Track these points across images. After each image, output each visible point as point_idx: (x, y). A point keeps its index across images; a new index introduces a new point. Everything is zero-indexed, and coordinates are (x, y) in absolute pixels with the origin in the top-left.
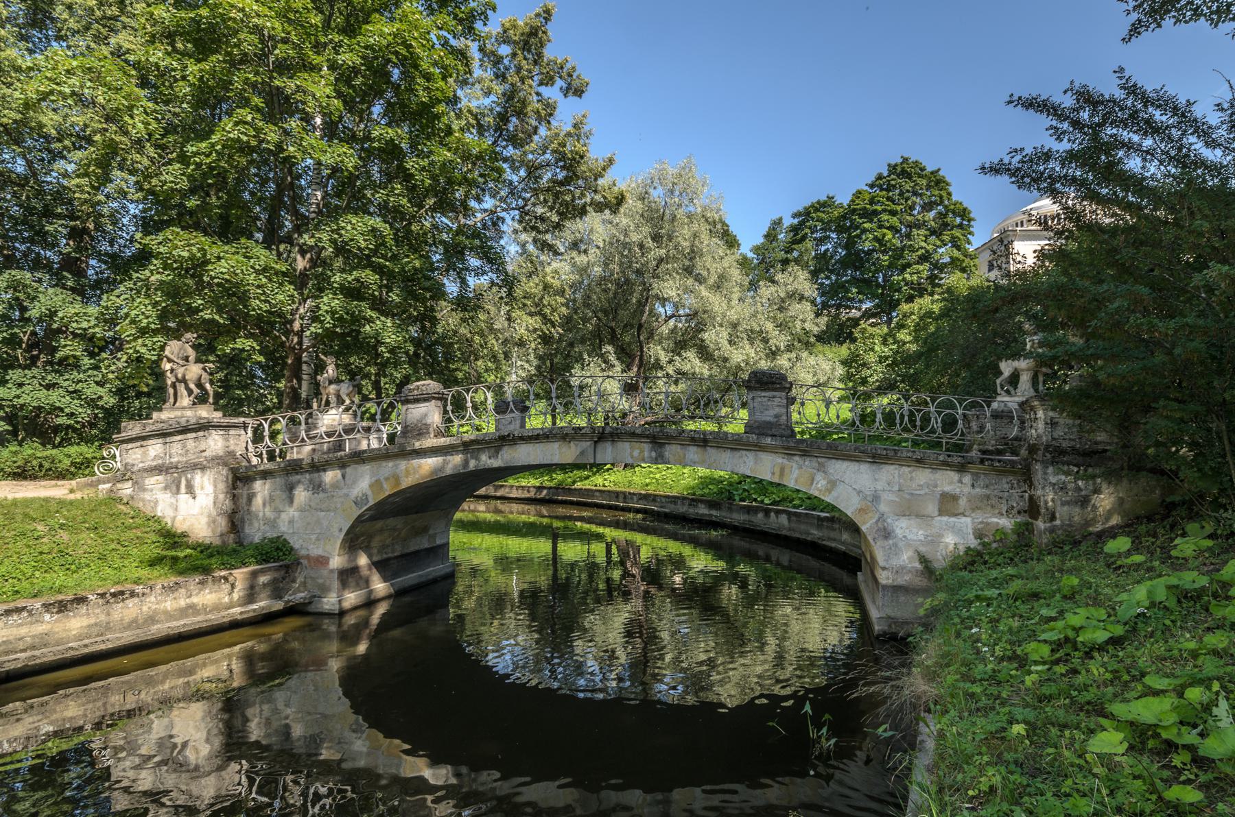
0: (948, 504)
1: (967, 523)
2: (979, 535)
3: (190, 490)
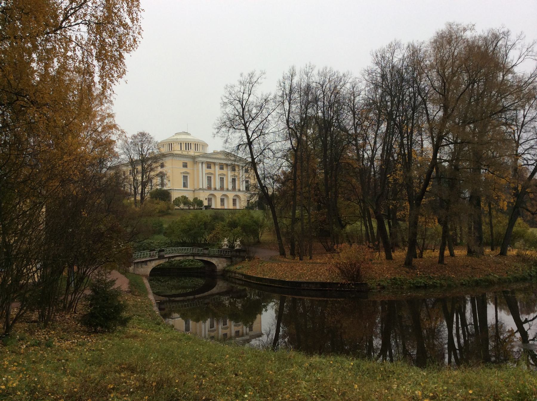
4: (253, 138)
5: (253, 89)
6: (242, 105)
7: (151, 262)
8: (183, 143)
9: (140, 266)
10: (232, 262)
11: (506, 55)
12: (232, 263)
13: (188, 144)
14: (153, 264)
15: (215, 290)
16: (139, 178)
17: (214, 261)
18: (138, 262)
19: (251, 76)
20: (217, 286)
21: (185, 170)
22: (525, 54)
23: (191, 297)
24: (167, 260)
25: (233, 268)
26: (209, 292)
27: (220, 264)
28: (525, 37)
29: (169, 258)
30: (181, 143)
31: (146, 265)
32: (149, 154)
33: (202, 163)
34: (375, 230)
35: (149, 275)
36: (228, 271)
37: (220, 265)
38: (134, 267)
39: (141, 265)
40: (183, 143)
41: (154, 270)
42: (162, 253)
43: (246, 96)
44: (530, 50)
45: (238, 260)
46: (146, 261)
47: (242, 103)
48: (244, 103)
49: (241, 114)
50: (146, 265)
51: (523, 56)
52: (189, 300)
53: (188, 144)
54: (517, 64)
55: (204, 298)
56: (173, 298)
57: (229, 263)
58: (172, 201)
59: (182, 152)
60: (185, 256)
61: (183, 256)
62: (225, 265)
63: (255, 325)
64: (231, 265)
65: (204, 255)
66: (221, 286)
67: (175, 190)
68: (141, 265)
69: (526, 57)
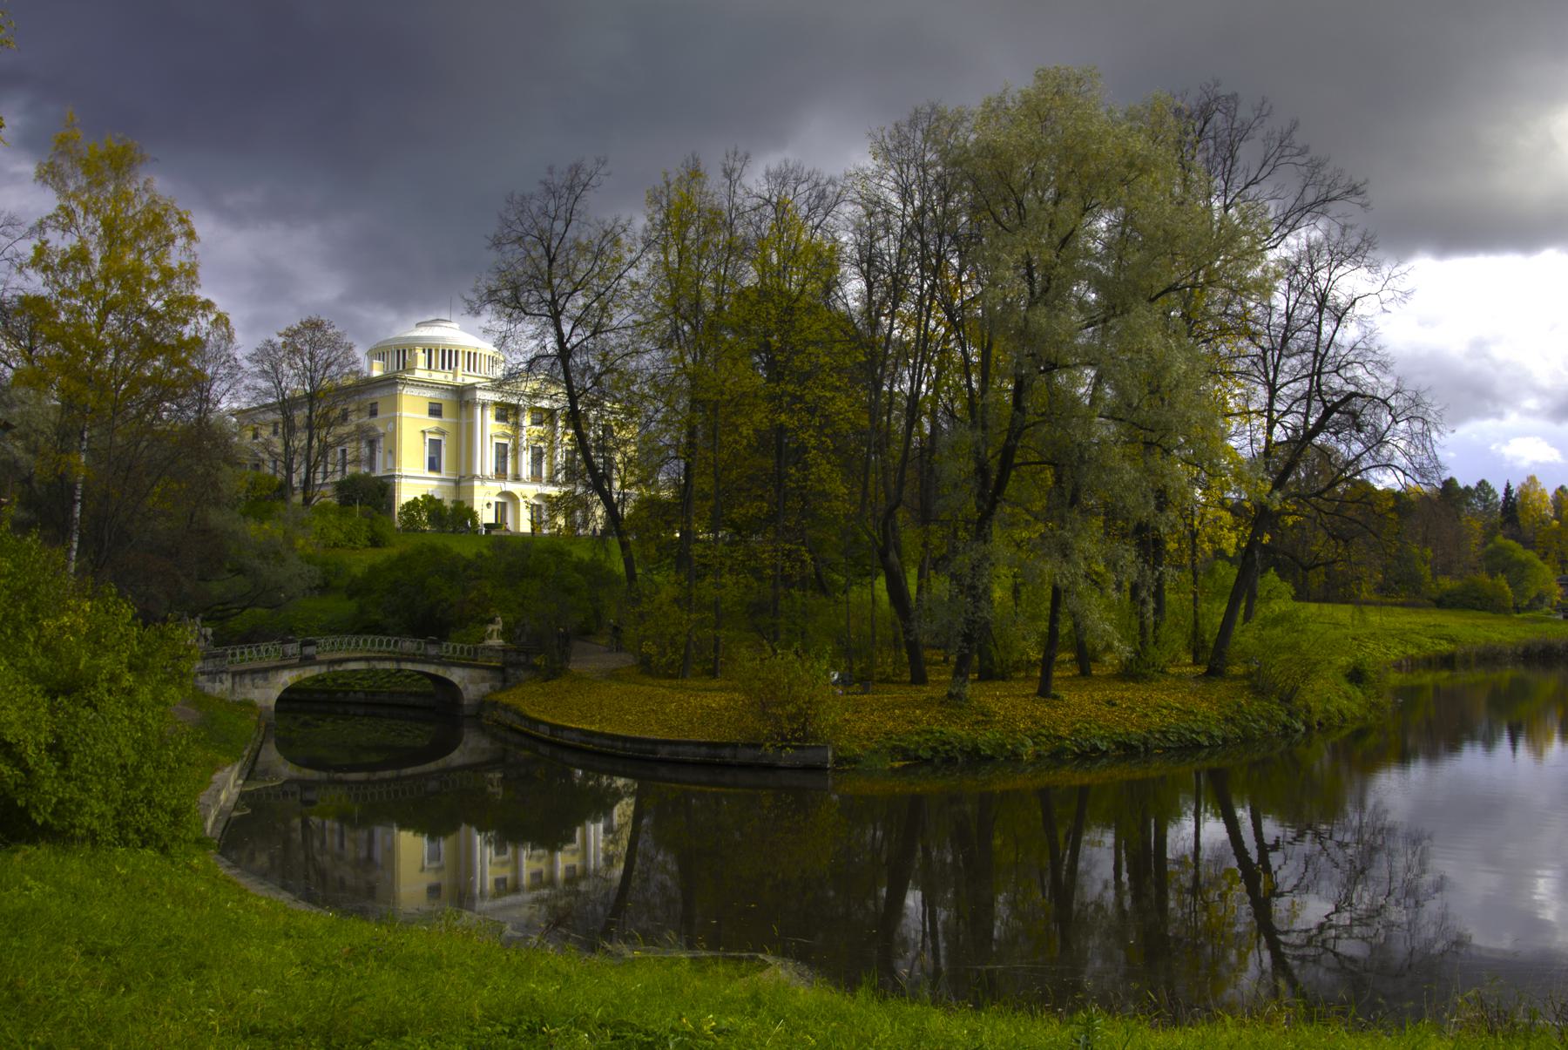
0: (483, 680)
1: (488, 685)
2: (491, 687)
3: (221, 681)
4: (574, 340)
5: (578, 207)
6: (548, 251)
7: (270, 675)
8: (437, 350)
9: (247, 680)
10: (505, 681)
11: (1232, 156)
12: (506, 684)
13: (450, 352)
14: (287, 678)
15: (456, 758)
16: (300, 440)
17: (456, 676)
18: (242, 673)
19: (576, 169)
20: (461, 746)
21: (433, 423)
22: (1277, 154)
23: (389, 774)
24: (324, 669)
25: (504, 698)
26: (441, 763)
27: (469, 683)
28: (1271, 107)
29: (332, 662)
30: (430, 351)
31: (266, 679)
32: (331, 378)
33: (484, 406)
34: (1243, 605)
35: (273, 709)
36: (495, 704)
37: (471, 687)
38: (233, 684)
39: (253, 680)
40: (437, 350)
41: (290, 699)
42: (310, 650)
43: (559, 226)
44: (1286, 142)
45: (522, 674)
46: (266, 671)
47: (549, 246)
48: (554, 244)
49: (546, 277)
50: (266, 679)
51: (1272, 161)
52: (382, 781)
53: (450, 352)
54: (1259, 178)
55: (427, 776)
56: (340, 775)
57: (499, 685)
58: (397, 510)
59: (430, 375)
60: (374, 659)
61: (367, 659)
62: (485, 687)
63: (1370, 802)
64: (502, 689)
65: (427, 660)
66: (471, 748)
67: (406, 477)
68: (253, 680)
69: (1282, 161)
